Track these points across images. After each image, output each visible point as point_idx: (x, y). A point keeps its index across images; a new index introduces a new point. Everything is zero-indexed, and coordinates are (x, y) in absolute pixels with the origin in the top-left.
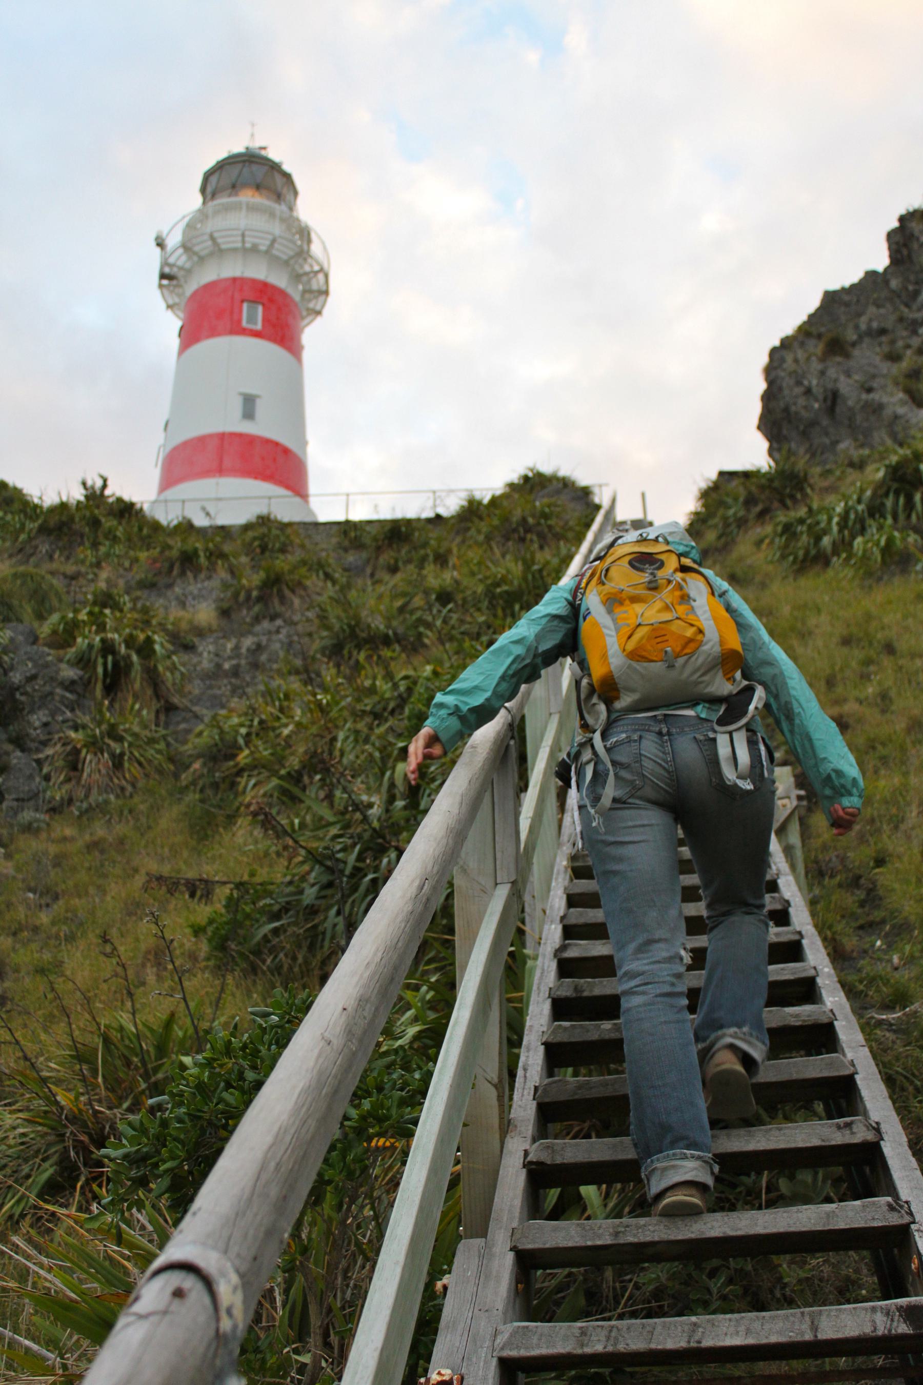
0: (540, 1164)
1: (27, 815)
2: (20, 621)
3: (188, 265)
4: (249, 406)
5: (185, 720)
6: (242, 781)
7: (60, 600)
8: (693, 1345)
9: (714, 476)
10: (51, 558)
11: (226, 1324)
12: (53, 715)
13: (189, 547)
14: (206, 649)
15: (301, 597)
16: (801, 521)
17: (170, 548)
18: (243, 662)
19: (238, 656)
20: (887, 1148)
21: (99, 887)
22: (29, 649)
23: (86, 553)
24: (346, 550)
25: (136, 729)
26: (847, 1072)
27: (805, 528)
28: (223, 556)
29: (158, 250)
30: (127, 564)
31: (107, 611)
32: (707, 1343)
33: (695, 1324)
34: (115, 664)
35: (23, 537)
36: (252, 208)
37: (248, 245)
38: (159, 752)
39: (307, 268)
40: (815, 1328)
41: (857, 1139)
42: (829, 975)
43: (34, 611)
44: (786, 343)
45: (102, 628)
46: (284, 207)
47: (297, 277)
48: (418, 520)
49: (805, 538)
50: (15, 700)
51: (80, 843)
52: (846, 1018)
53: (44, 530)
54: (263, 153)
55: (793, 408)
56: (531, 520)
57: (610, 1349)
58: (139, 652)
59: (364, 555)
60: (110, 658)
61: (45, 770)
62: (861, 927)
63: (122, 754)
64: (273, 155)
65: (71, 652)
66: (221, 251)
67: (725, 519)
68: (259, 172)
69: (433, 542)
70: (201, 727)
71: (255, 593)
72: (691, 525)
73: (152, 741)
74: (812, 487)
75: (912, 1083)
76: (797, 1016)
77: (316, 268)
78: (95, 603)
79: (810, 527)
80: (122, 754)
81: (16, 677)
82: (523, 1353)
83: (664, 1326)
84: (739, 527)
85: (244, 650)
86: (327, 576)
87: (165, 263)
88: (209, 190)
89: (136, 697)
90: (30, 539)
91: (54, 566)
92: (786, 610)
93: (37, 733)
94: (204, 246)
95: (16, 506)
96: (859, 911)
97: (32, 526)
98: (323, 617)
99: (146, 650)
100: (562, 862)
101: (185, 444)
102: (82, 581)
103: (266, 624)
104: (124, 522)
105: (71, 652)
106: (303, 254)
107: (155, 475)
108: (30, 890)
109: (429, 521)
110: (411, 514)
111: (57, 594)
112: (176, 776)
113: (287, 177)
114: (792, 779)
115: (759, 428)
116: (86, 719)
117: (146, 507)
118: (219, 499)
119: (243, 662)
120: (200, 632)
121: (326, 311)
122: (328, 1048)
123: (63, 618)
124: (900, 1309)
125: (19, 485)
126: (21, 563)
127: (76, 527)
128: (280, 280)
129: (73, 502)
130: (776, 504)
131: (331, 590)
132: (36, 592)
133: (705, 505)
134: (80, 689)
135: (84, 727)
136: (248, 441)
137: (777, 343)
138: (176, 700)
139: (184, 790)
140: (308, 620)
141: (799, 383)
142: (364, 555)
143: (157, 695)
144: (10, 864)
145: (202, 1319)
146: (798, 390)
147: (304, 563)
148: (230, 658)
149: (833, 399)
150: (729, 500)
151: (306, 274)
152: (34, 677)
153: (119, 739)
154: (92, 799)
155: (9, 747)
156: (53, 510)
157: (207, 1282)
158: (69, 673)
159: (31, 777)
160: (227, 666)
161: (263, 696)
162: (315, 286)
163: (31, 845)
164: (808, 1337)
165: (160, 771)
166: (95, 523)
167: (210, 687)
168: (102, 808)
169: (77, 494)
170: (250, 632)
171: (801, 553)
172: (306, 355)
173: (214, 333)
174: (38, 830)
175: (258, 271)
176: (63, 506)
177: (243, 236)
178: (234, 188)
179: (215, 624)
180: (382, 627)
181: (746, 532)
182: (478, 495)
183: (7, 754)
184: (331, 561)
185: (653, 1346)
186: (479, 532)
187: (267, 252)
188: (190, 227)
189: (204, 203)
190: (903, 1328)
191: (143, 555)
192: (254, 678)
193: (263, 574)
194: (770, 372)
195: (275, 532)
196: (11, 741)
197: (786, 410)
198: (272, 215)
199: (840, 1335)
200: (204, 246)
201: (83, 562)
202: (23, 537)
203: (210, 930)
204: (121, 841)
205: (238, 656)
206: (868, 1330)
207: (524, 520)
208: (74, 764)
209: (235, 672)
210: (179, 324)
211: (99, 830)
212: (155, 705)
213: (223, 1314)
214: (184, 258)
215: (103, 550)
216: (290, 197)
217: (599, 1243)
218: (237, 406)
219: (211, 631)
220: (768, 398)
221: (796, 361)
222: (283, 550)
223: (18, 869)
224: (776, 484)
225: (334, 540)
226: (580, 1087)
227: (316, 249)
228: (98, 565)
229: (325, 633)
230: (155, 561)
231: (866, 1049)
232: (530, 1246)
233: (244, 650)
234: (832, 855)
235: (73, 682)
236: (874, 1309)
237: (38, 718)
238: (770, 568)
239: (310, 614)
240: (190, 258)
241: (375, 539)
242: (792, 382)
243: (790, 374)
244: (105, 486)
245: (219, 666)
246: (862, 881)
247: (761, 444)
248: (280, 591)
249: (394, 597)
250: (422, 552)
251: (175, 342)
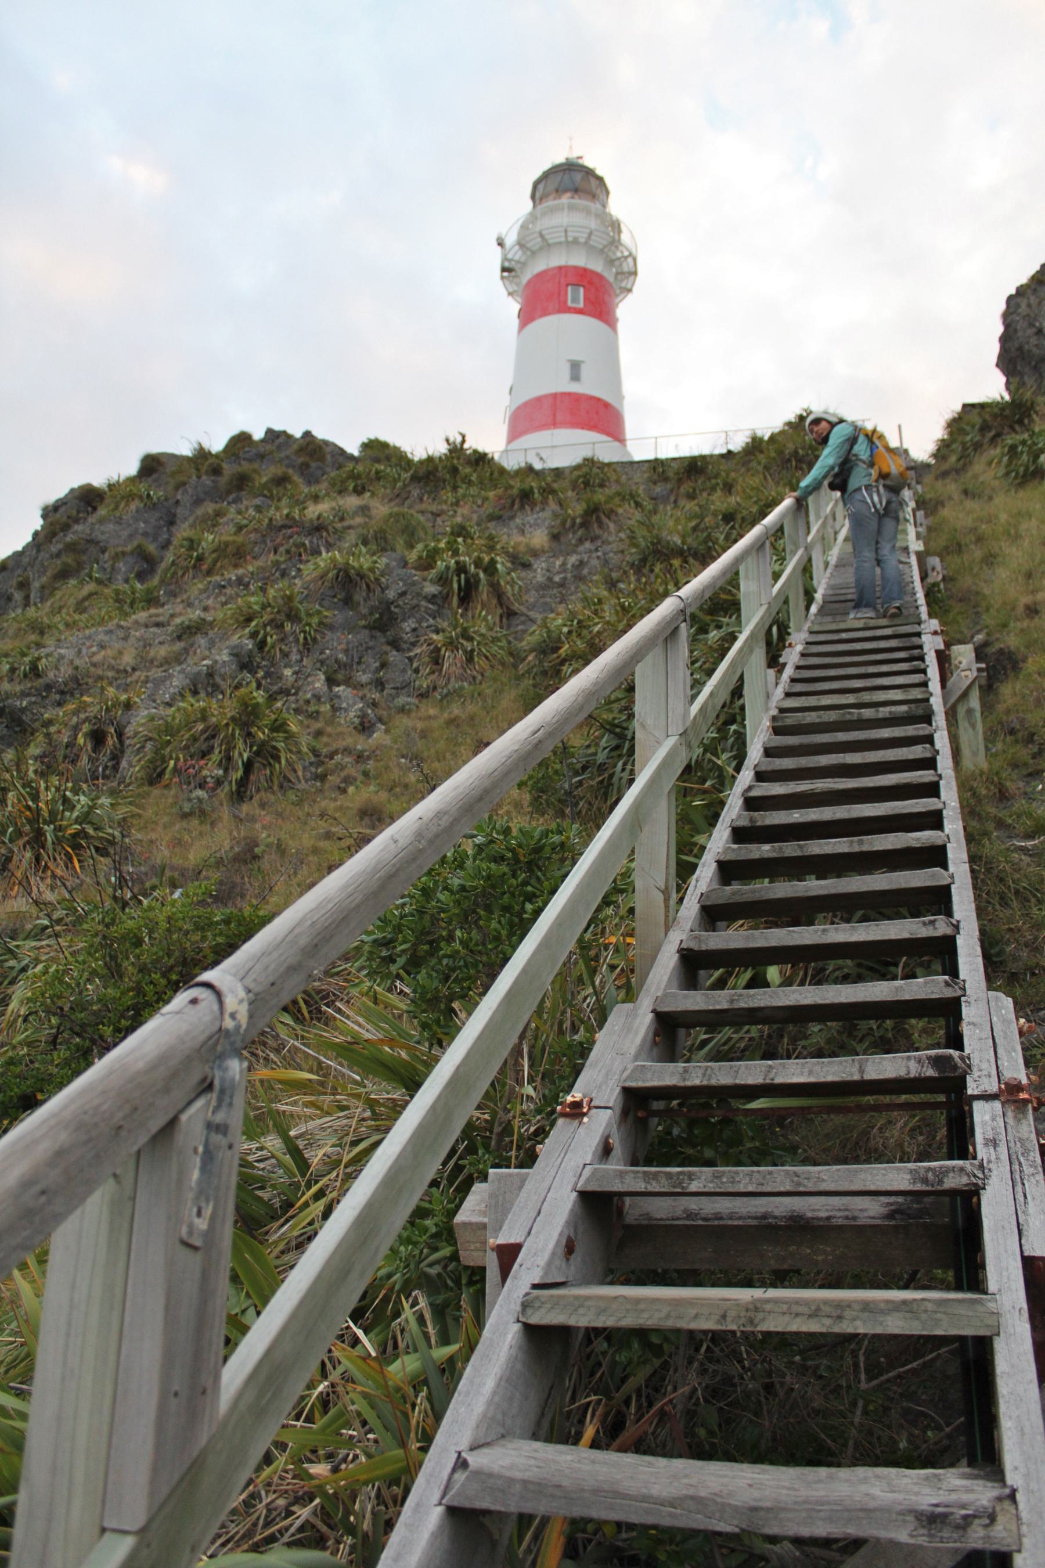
0: (690, 950)
1: (402, 700)
2: (393, 550)
3: (523, 259)
4: (575, 370)
5: (523, 623)
6: (564, 668)
7: (426, 533)
8: (768, 1081)
9: (958, 408)
10: (421, 500)
11: (229, 1024)
12: (419, 622)
13: (526, 486)
14: (540, 566)
15: (615, 522)
16: (1023, 443)
17: (511, 487)
18: (569, 575)
19: (565, 571)
20: (960, 941)
21: (454, 753)
22: (400, 571)
23: (448, 495)
24: (655, 483)
25: (483, 631)
26: (945, 883)
27: (1026, 449)
28: (553, 492)
29: (499, 248)
30: (480, 502)
31: (460, 540)
32: (779, 1080)
33: (770, 1066)
34: (467, 580)
35: (399, 485)
36: (571, 208)
37: (570, 239)
38: (501, 648)
39: (619, 254)
40: (862, 1071)
41: (939, 933)
42: (954, 808)
43: (406, 542)
44: (1021, 291)
45: (456, 553)
46: (598, 206)
47: (611, 262)
48: (711, 456)
49: (1025, 457)
50: (391, 612)
51: (441, 721)
52: (958, 841)
53: (415, 478)
54: (580, 161)
55: (1026, 347)
56: (801, 452)
57: (705, 1083)
58: (485, 571)
59: (669, 486)
60: (463, 576)
61: (415, 665)
62: (1030, 775)
63: (473, 651)
64: (588, 162)
65: (433, 573)
66: (549, 245)
67: (964, 444)
68: (578, 177)
69: (723, 474)
70: (534, 628)
71: (578, 521)
72: (938, 450)
73: (495, 640)
74: (1036, 413)
75: (1035, 896)
76: (918, 839)
77: (626, 254)
78: (452, 533)
79: (1030, 447)
80: (473, 651)
81: (391, 594)
82: (640, 1084)
83: (747, 1067)
84: (975, 450)
85: (569, 566)
86: (638, 505)
87: (505, 259)
88: (538, 196)
89: (483, 607)
90: (405, 486)
91: (423, 506)
92: (1003, 517)
93: (409, 637)
94: (535, 243)
95: (394, 460)
96: (1031, 762)
97: (406, 476)
98: (632, 538)
99: (490, 569)
100: (767, 723)
101: (526, 404)
102: (444, 517)
103: (588, 545)
104: (479, 469)
105: (433, 573)
106: (615, 242)
107: (503, 430)
108: (403, 757)
109: (722, 456)
110: (706, 451)
111: (423, 528)
112: (515, 666)
113: (600, 179)
114: (973, 655)
115: (997, 365)
116: (445, 624)
117: (496, 457)
118: (554, 447)
119: (569, 575)
120: (535, 553)
121: (634, 289)
122: (393, 846)
123: (426, 546)
124: (929, 1058)
125: (398, 444)
126: (398, 505)
127: (439, 475)
128: (596, 266)
129: (437, 454)
130: (1006, 430)
131: (638, 515)
132: (407, 527)
133: (951, 434)
134: (439, 602)
135: (443, 631)
136: (575, 398)
137: (1013, 292)
138: (516, 606)
139: (519, 678)
140: (621, 540)
141: (1031, 325)
142: (669, 486)
143: (501, 604)
144: (388, 737)
145: (207, 1018)
146: (1031, 331)
147: (618, 494)
148: (558, 573)
150: (968, 428)
151: (619, 259)
152: (403, 594)
153: (470, 639)
154: (450, 687)
155: (388, 648)
156: (421, 462)
157: (218, 994)
158: (431, 589)
159: (404, 671)
160: (557, 579)
162: (625, 269)
163: (403, 722)
164: (856, 1077)
165: (503, 664)
166: (455, 471)
167: (543, 596)
168: (458, 693)
169: (442, 449)
170: (575, 552)
171: (1022, 470)
172: (620, 326)
173: (545, 313)
174: (410, 711)
175: (579, 259)
176: (430, 459)
177: (566, 231)
178: (559, 191)
179: (547, 546)
180: (679, 542)
181: (981, 454)
182: (759, 434)
183: (386, 653)
184: (640, 492)
185: (738, 1081)
186: (759, 463)
187: (586, 243)
188: (524, 227)
189: (534, 206)
190: (930, 1072)
191: (491, 494)
192: (577, 588)
193: (584, 506)
194: (1006, 316)
195: (595, 470)
196: (389, 643)
197: (1020, 349)
198: (588, 212)
199: (881, 1077)
200: (535, 243)
201: (446, 502)
202: (399, 485)
203: (530, 783)
204: (472, 718)
205: (565, 571)
206: (902, 1073)
207: (796, 452)
208: (436, 660)
209: (562, 585)
210: (517, 307)
211: (456, 710)
212: (499, 611)
213: (227, 1016)
214: (520, 253)
215: (461, 491)
216: (602, 196)
217: (718, 1007)
218: (566, 372)
219: (543, 551)
220: (1004, 339)
221: (1029, 306)
222: (602, 485)
223: (395, 742)
224: (1007, 412)
225: (646, 475)
226: (733, 894)
227: (625, 237)
228: (457, 504)
229: (634, 550)
230: (500, 498)
231: (967, 866)
232: (666, 1009)
233: (569, 566)
234: (1012, 717)
235: (434, 596)
236: (909, 1058)
237: (408, 625)
238: (997, 482)
239: (622, 535)
240: (524, 253)
241: (677, 474)
242: (1025, 324)
243: (1024, 317)
244: (463, 441)
245: (550, 579)
246: (1036, 738)
248: (598, 518)
249: (691, 519)
250: (714, 481)
251: (516, 322)
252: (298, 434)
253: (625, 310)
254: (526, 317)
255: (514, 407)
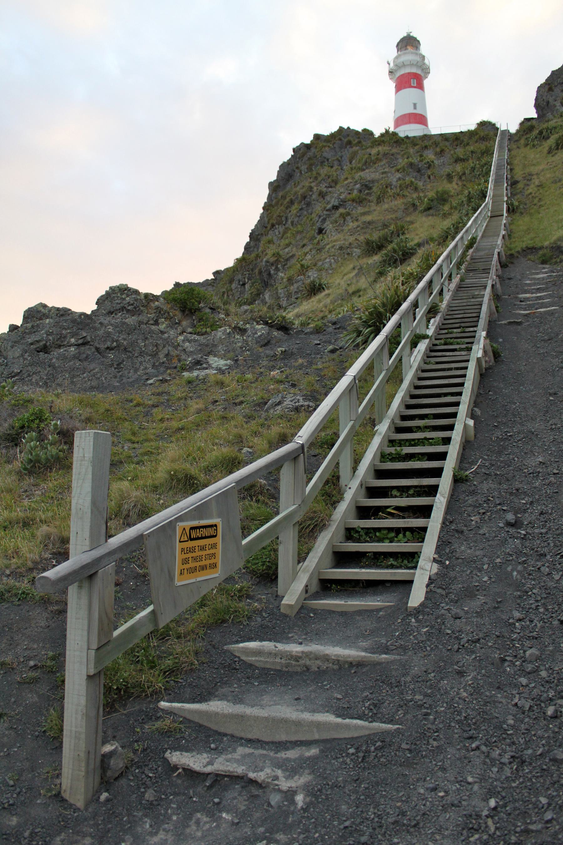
101: (401, 116)
113: (418, 41)
128: (419, 72)
136: (415, 115)
149: (548, 102)
161: (74, 377)
173: (405, 88)
175: (414, 70)
210: (394, 85)
220: (536, 99)
227: (426, 61)
247: (534, 110)
251: (394, 90)
252: (346, 128)
253: (426, 83)
254: (398, 88)
255: (396, 117)
